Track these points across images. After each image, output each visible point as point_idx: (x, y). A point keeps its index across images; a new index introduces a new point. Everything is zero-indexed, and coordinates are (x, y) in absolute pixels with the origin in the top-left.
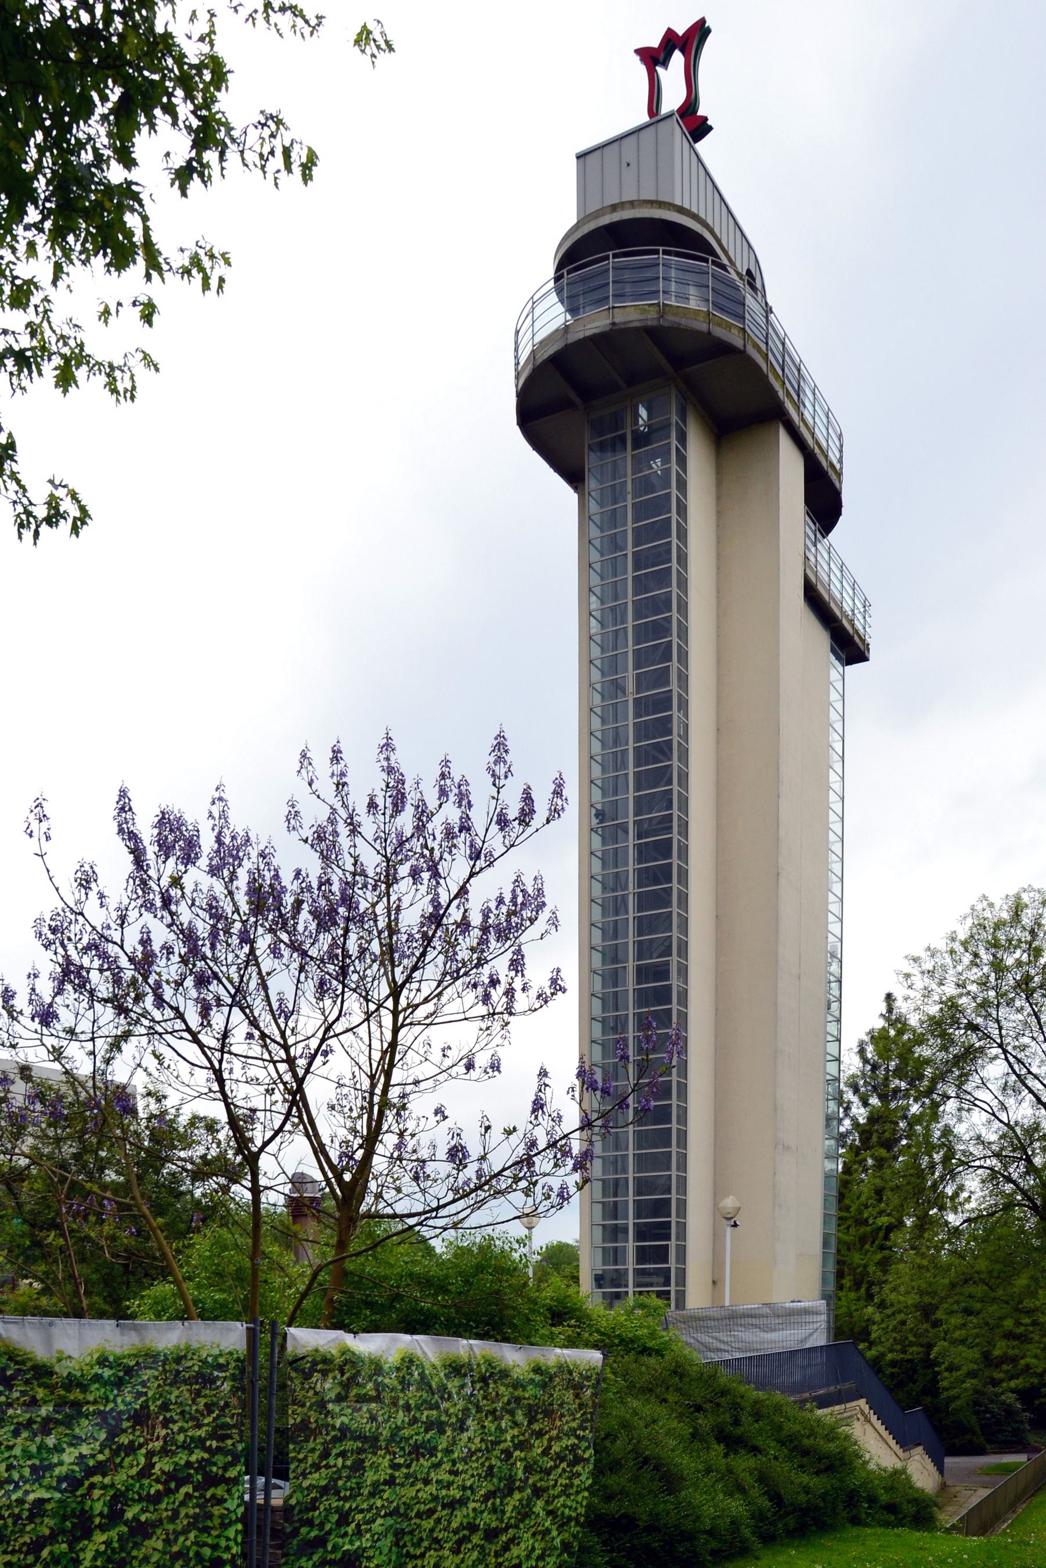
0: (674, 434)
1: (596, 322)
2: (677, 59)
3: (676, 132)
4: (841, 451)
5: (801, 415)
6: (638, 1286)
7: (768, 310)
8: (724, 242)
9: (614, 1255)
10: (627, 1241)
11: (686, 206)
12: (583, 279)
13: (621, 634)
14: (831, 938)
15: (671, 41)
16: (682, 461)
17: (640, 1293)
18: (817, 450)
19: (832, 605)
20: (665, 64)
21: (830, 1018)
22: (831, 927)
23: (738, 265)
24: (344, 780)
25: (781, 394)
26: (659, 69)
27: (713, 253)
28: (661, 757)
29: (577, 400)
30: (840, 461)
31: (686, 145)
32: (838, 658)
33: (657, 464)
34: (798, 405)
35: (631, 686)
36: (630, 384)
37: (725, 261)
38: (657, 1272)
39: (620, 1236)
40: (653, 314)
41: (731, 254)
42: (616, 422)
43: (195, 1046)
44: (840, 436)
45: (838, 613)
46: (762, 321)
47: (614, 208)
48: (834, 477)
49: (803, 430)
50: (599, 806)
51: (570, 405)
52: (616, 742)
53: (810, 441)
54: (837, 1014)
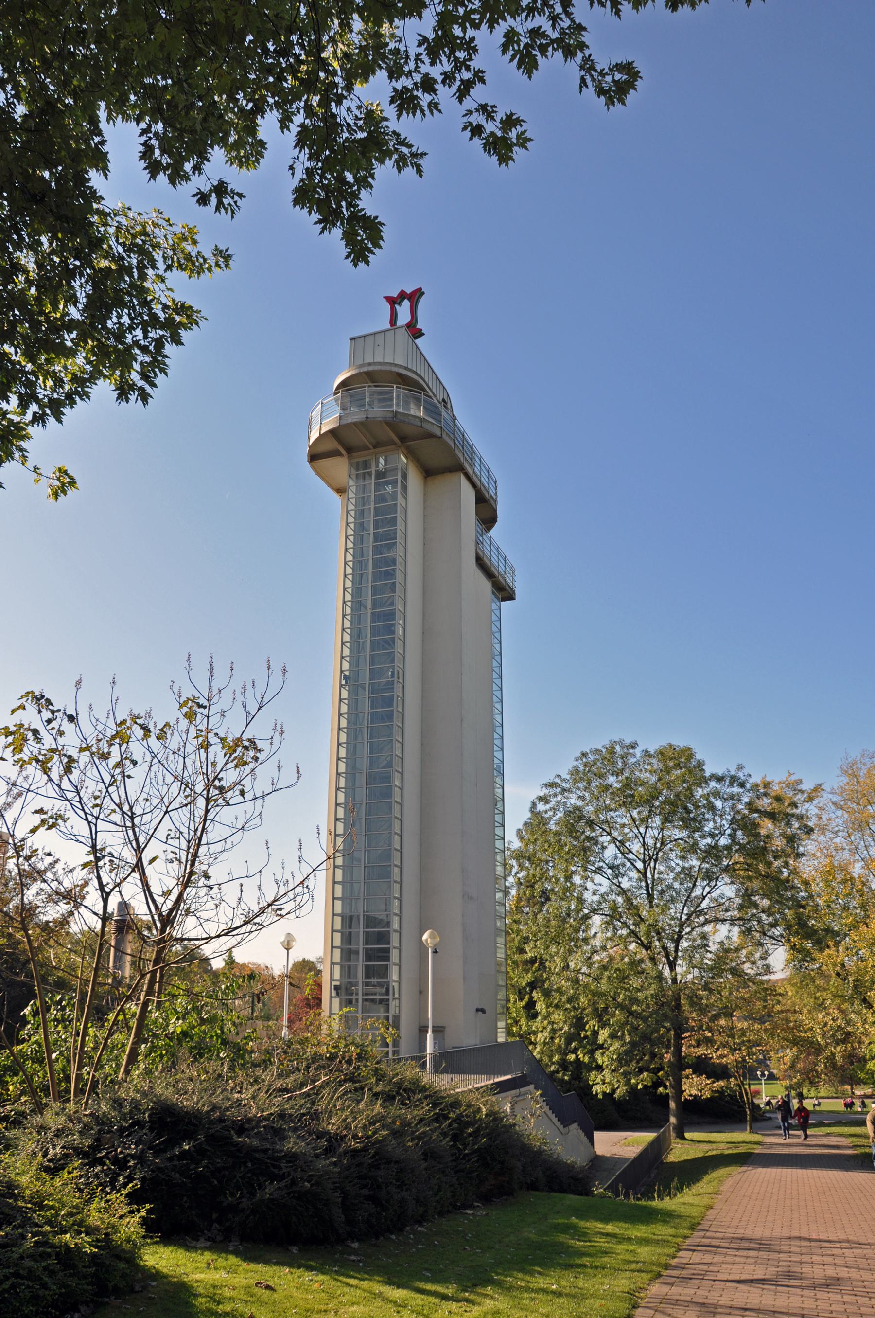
0: (399, 474)
1: (357, 415)
2: (406, 303)
3: (403, 335)
4: (496, 489)
5: (473, 470)
6: (367, 994)
7: (454, 419)
8: (430, 385)
9: (348, 971)
10: (358, 961)
11: (410, 367)
12: (347, 390)
13: (364, 576)
14: (496, 761)
15: (403, 295)
16: (405, 488)
17: (366, 1000)
18: (482, 488)
19: (493, 568)
20: (400, 304)
21: (497, 812)
22: (496, 754)
23: (438, 396)
24: (133, 397)
25: (462, 459)
26: (397, 306)
27: (424, 390)
28: (387, 646)
29: (344, 452)
30: (496, 494)
31: (410, 340)
32: (497, 597)
33: (389, 488)
34: (472, 466)
35: (369, 605)
36: (375, 447)
37: (431, 394)
38: (380, 985)
39: (353, 957)
40: (391, 415)
41: (434, 391)
42: (366, 465)
43: (86, 822)
44: (496, 482)
45: (496, 573)
46: (451, 424)
47: (370, 364)
48: (492, 502)
49: (474, 477)
50: (347, 673)
51: (341, 455)
52: (359, 636)
53: (478, 483)
54: (501, 809)
